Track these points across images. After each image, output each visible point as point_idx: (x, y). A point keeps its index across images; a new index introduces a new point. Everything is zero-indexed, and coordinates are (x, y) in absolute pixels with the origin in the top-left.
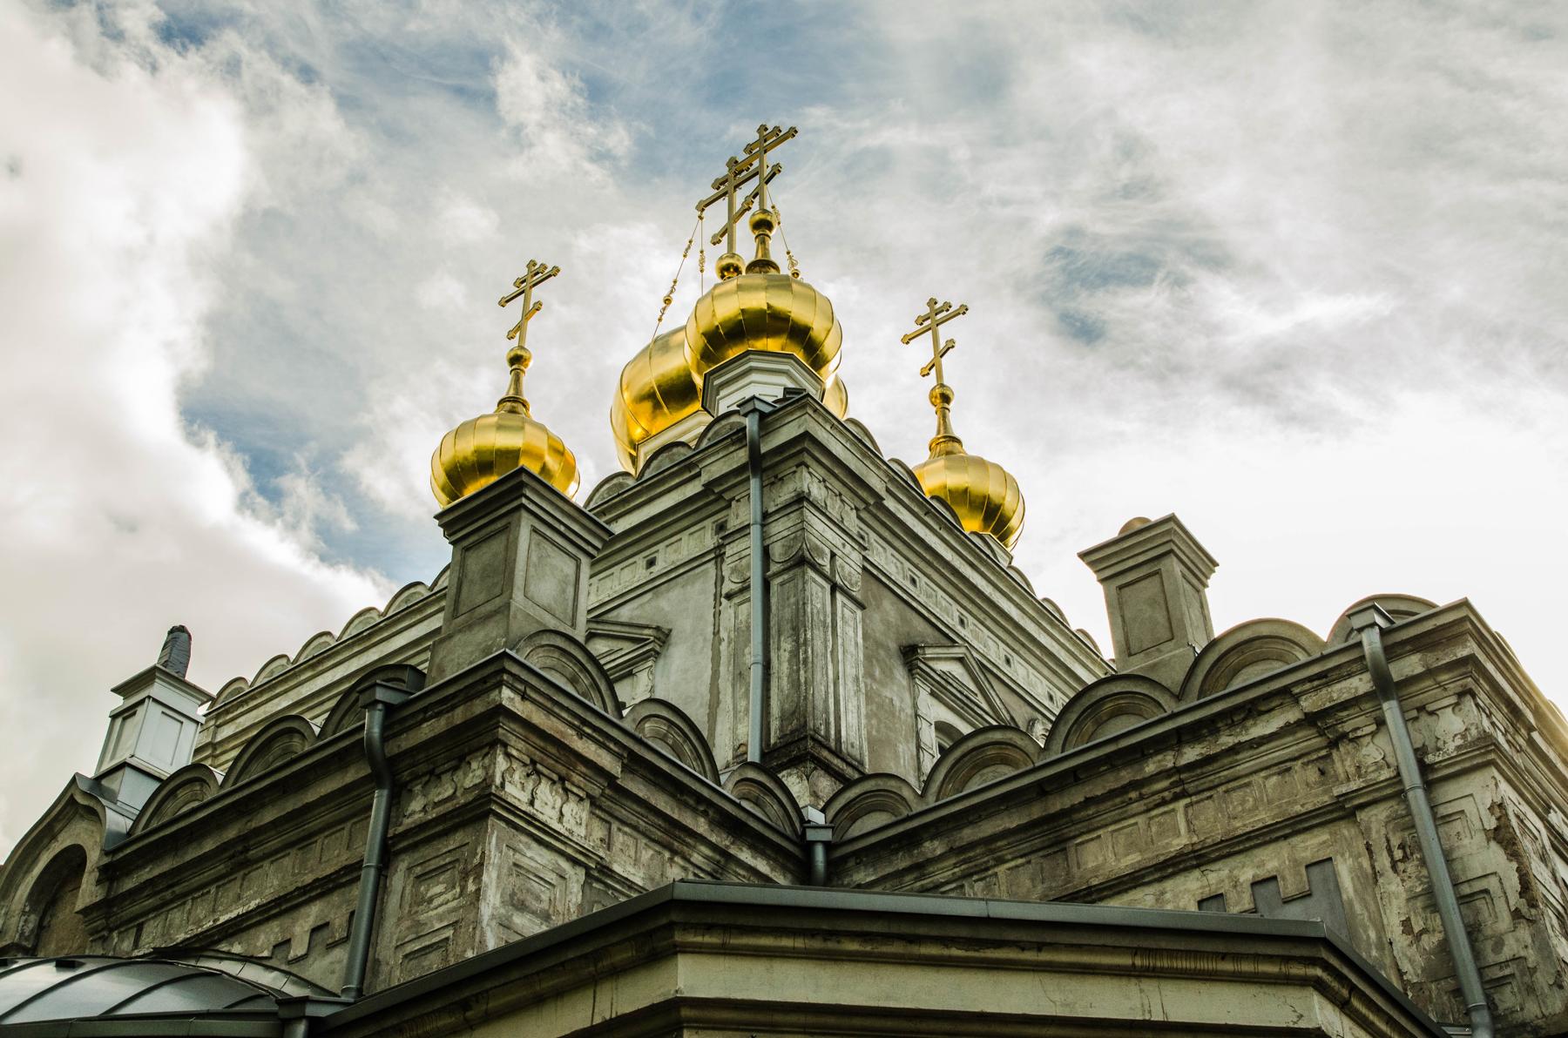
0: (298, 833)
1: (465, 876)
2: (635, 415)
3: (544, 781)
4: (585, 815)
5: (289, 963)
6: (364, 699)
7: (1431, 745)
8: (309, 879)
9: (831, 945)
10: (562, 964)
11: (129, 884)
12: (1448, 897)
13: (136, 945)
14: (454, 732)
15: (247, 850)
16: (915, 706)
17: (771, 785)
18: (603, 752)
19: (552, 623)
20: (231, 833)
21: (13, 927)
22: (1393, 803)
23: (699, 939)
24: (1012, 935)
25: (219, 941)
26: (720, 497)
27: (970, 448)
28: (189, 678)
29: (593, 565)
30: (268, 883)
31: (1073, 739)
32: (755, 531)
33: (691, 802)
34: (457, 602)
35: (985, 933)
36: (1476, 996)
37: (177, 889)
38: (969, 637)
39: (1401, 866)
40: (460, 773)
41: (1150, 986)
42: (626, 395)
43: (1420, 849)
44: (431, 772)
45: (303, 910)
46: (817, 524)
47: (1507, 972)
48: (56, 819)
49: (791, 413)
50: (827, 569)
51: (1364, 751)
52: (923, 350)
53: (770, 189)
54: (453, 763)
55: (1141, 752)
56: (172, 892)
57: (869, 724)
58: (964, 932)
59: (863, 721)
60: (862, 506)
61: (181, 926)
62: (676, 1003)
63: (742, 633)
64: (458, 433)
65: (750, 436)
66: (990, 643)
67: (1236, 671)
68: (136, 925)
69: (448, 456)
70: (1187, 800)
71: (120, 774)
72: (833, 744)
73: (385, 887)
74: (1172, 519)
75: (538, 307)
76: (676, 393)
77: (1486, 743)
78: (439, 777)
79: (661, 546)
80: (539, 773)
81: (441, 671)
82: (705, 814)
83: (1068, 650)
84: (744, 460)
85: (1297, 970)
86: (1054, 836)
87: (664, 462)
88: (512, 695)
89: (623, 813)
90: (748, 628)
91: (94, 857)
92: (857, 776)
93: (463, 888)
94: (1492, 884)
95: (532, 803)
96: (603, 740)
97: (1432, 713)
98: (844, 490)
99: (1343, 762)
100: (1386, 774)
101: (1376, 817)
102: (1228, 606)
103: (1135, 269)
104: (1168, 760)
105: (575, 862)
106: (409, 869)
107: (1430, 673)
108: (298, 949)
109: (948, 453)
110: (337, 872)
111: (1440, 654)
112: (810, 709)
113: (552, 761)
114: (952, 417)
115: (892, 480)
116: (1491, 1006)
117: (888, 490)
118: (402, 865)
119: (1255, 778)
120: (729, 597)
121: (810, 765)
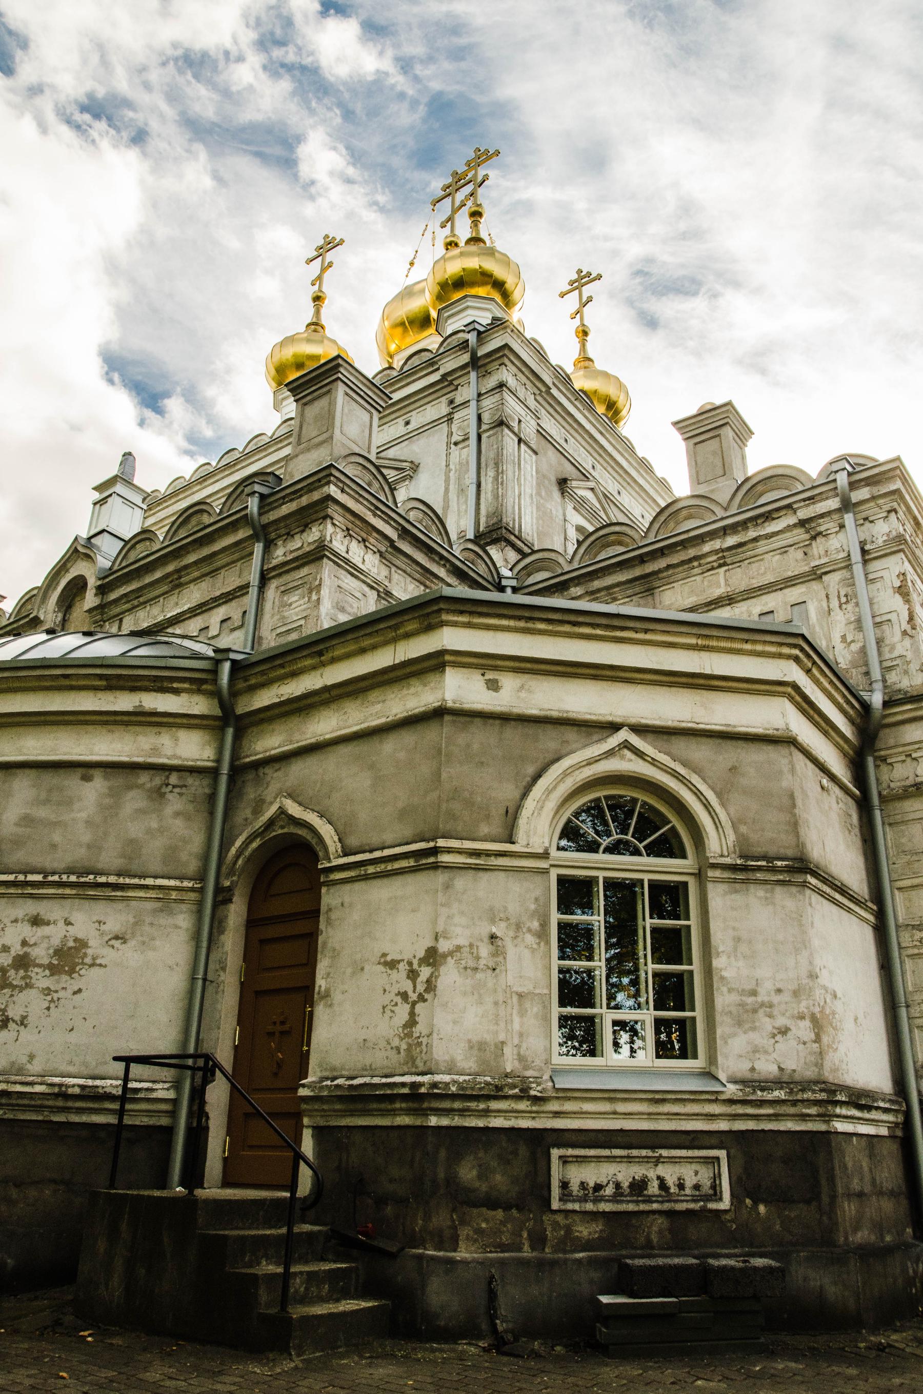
0: (210, 567)
1: (310, 591)
2: (392, 336)
3: (354, 540)
4: (377, 562)
5: (209, 639)
6: (248, 490)
7: (869, 539)
8: (218, 593)
9: (530, 625)
10: (377, 631)
11: (113, 596)
12: (868, 623)
13: (120, 628)
14: (301, 510)
15: (180, 577)
16: (564, 515)
17: (481, 553)
18: (387, 526)
19: (357, 450)
20: (170, 568)
21: (49, 619)
22: (844, 571)
23: (455, 618)
24: (631, 624)
25: (167, 627)
26: (451, 383)
27: (599, 365)
28: (136, 482)
29: (380, 419)
30: (193, 596)
31: (661, 531)
32: (473, 404)
33: (437, 559)
34: (299, 436)
35: (616, 622)
36: (876, 674)
37: (141, 600)
38: (597, 477)
39: (844, 606)
40: (305, 534)
41: (705, 655)
42: (386, 323)
43: (856, 597)
44: (288, 534)
45: (215, 611)
46: (510, 400)
47: (895, 663)
48: (67, 560)
49: (497, 332)
50: (516, 430)
51: (830, 542)
52: (572, 301)
53: (480, 191)
54: (302, 528)
55: (701, 539)
56: (137, 601)
57: (538, 523)
58: (604, 621)
59: (535, 521)
60: (537, 392)
61: (145, 618)
62: (442, 653)
63: (464, 465)
64: (283, 344)
65: (467, 350)
66: (610, 481)
67: (761, 495)
68: (119, 618)
69: (276, 358)
70: (726, 568)
71: (102, 535)
72: (517, 533)
73: (263, 598)
74: (729, 404)
75: (330, 265)
76: (423, 322)
77: (900, 539)
78: (292, 536)
79: (414, 413)
80: (351, 536)
81: (292, 476)
82: (444, 566)
83: (655, 489)
84: (467, 361)
85: (786, 650)
86: (647, 586)
87: (416, 361)
88: (336, 489)
89: (398, 563)
90: (468, 462)
91: (92, 582)
92: (530, 551)
93: (309, 598)
94: (893, 617)
95: (347, 552)
96: (388, 519)
97: (872, 522)
98: (528, 382)
99: (818, 547)
100: (843, 555)
101: (833, 580)
102: (757, 458)
103: (684, 286)
104: (717, 544)
105: (372, 588)
106: (277, 588)
107: (873, 498)
108: (213, 632)
109: (585, 368)
110: (234, 590)
111: (880, 488)
112: (504, 511)
113: (359, 528)
114: (589, 346)
115: (557, 377)
116: (884, 681)
117: (554, 384)
118: (273, 585)
119: (766, 556)
120: (456, 444)
121: (503, 544)
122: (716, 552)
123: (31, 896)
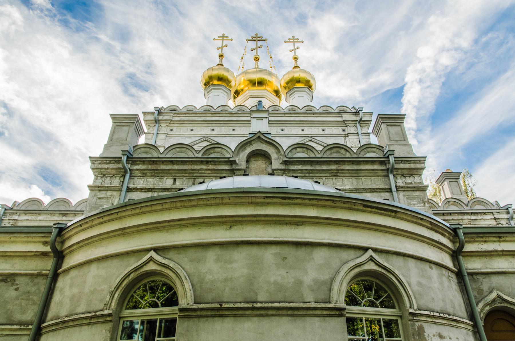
15: (337, 173)
37: (311, 175)
104: (469, 217)
122: (468, 219)
123: (435, 323)
